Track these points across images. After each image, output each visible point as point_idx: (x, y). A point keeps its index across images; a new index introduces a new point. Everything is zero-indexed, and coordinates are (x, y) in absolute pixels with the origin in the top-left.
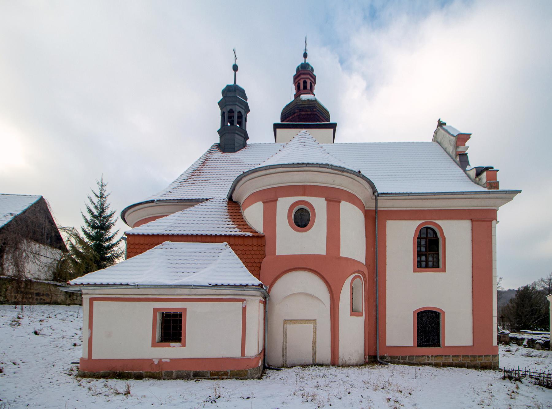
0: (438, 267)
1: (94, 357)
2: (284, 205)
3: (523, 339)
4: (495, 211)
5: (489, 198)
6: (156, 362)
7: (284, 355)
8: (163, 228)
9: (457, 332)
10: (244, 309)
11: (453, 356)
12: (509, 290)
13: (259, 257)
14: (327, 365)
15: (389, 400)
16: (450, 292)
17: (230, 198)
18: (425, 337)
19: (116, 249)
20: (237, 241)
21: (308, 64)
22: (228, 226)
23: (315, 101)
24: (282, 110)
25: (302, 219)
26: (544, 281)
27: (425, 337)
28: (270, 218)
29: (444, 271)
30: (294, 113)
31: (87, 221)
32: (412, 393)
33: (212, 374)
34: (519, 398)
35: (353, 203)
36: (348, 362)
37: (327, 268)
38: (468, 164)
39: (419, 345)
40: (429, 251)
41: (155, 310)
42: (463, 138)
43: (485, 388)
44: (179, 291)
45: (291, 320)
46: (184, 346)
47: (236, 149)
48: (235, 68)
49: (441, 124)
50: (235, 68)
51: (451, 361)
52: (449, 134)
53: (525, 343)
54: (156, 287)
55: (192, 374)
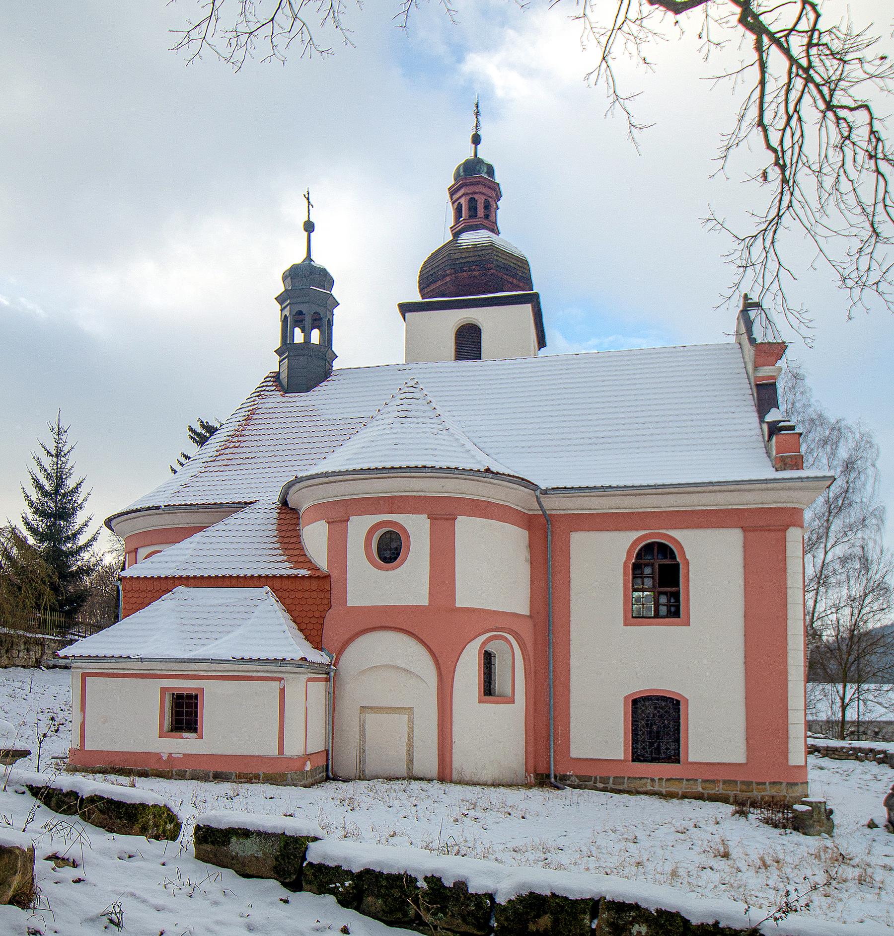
2: (359, 528)
5: (773, 489)
6: (165, 757)
7: (362, 761)
8: (174, 565)
9: (715, 736)
10: (282, 691)
11: (704, 781)
16: (699, 661)
17: (284, 503)
18: (651, 744)
19: (85, 555)
20: (285, 585)
21: (481, 161)
22: (275, 558)
27: (651, 744)
28: (338, 548)
30: (444, 276)
31: (31, 504)
32: (527, 816)
37: (436, 626)
41: (163, 690)
44: (193, 666)
45: (371, 708)
51: (700, 790)
55: (211, 775)
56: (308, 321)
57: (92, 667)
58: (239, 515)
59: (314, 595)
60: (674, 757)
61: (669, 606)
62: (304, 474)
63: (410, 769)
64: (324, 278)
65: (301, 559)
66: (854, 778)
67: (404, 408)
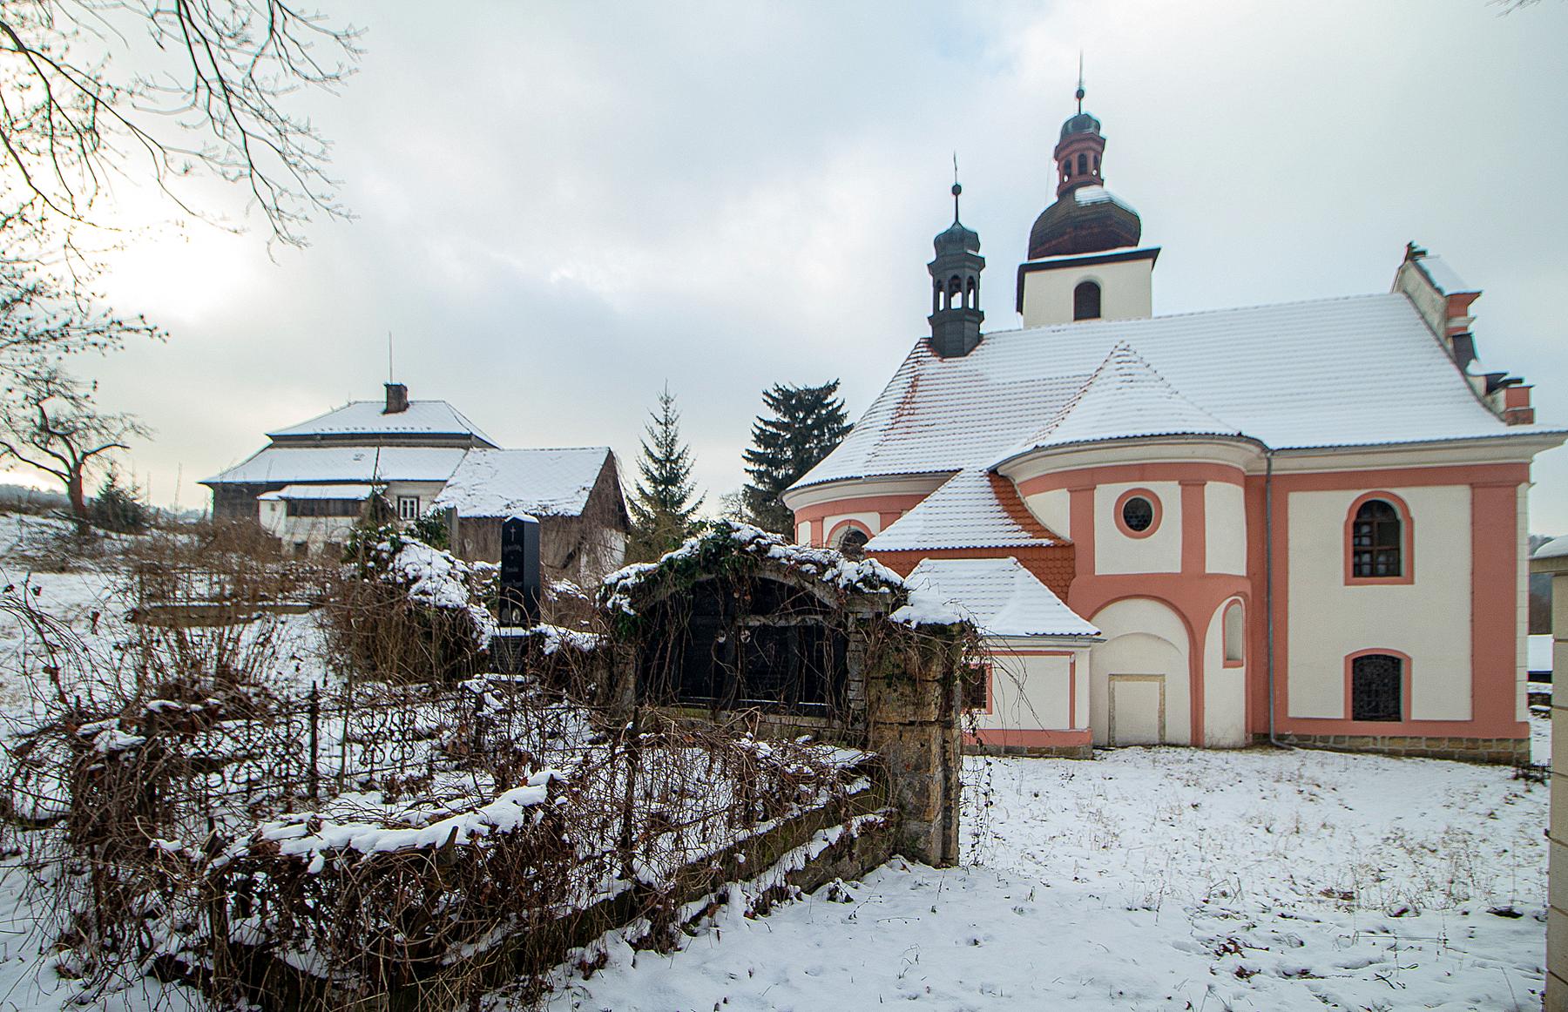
0: (1399, 575)
2: (1107, 497)
9: (1438, 692)
10: (1073, 665)
13: (1066, 577)
16: (1424, 619)
21: (1087, 116)
25: (1138, 517)
28: (1083, 516)
29: (1410, 581)
33: (1029, 751)
36: (1222, 743)
37: (1183, 594)
38: (1473, 355)
40: (1377, 544)
49: (1413, 254)
50: (957, 190)
52: (1431, 284)
56: (965, 285)
58: (950, 483)
59: (1059, 564)
60: (1395, 715)
61: (1387, 564)
62: (1046, 443)
63: (1162, 736)
64: (972, 239)
67: (1126, 371)
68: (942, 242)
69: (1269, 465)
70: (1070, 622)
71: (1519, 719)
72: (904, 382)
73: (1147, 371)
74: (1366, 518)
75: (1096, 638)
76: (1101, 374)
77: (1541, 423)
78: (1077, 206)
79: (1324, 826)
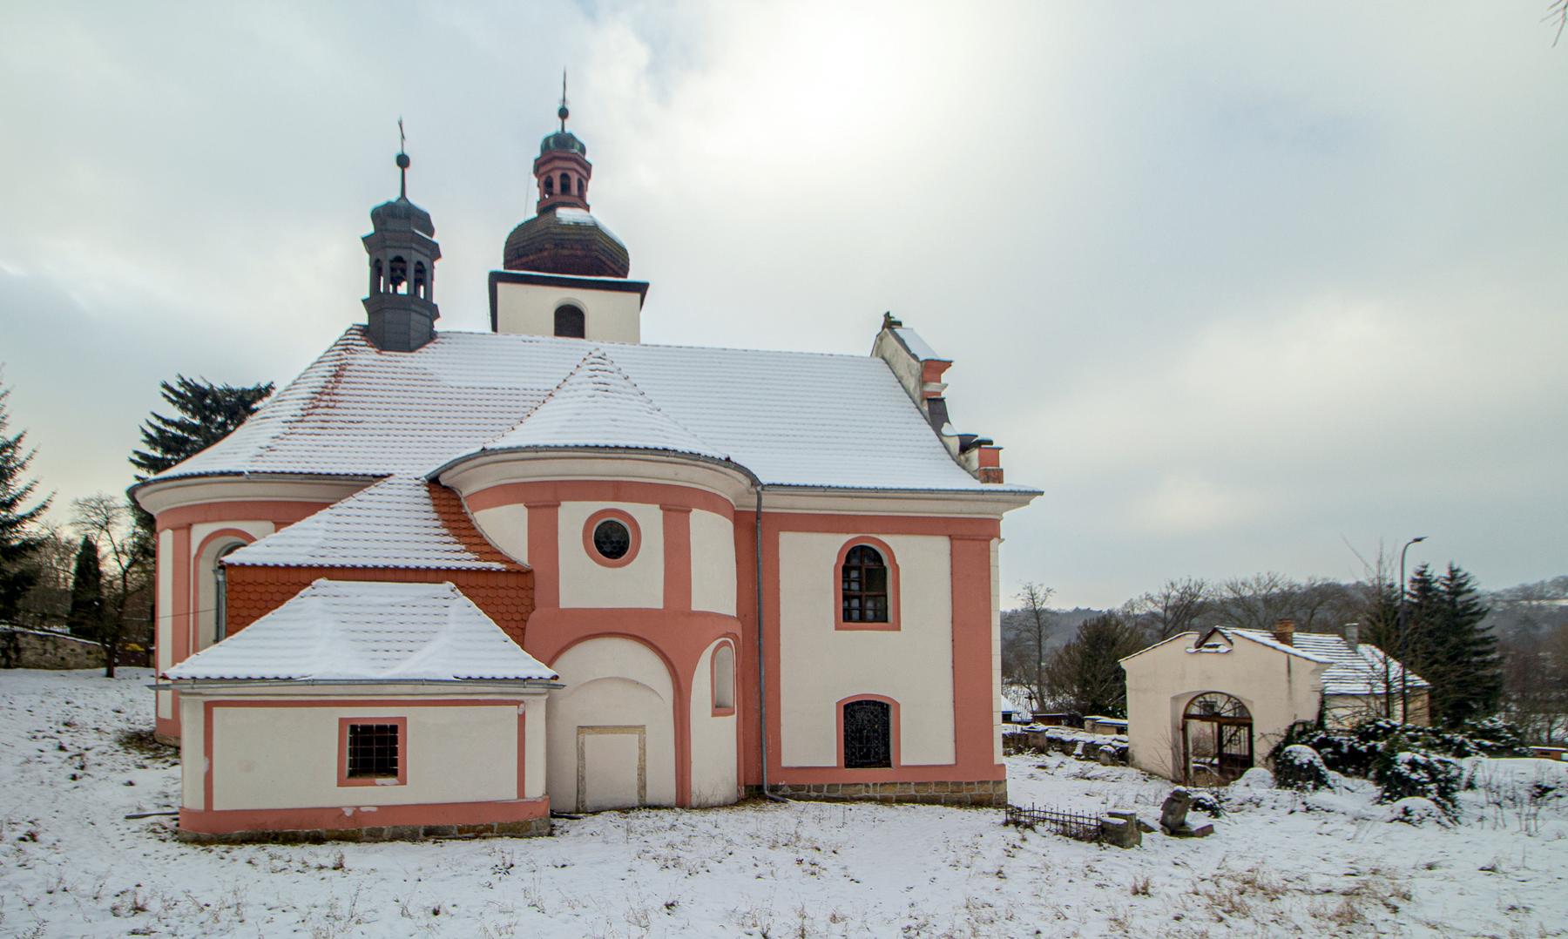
0: (886, 621)
1: (217, 807)
2: (574, 518)
3: (1074, 743)
4: (995, 524)
6: (349, 813)
9: (925, 739)
10: (522, 718)
12: (1077, 610)
13: (522, 609)
14: (669, 807)
15: (800, 862)
16: (909, 664)
20: (473, 580)
21: (571, 137)
22: (447, 547)
23: (595, 228)
24: (506, 236)
25: (612, 543)
26: (1152, 600)
27: (861, 749)
28: (544, 537)
33: (461, 830)
34: (1020, 854)
35: (715, 510)
36: (711, 801)
37: (666, 633)
39: (850, 763)
40: (865, 589)
41: (342, 721)
42: (934, 368)
43: (967, 840)
45: (592, 728)
46: (403, 782)
47: (413, 344)
48: (403, 161)
49: (890, 324)
50: (403, 161)
52: (908, 351)
53: (1078, 750)
54: (360, 682)
55: (421, 832)
57: (223, 692)
58: (372, 489)
59: (512, 593)
60: (885, 761)
62: (497, 446)
65: (486, 549)
66: (1126, 777)
68: (382, 216)
69: (759, 499)
70: (529, 666)
71: (997, 762)
72: (325, 370)
73: (624, 383)
74: (855, 562)
75: (552, 684)
76: (572, 380)
77: (1011, 481)
78: (558, 223)
79: (834, 919)
